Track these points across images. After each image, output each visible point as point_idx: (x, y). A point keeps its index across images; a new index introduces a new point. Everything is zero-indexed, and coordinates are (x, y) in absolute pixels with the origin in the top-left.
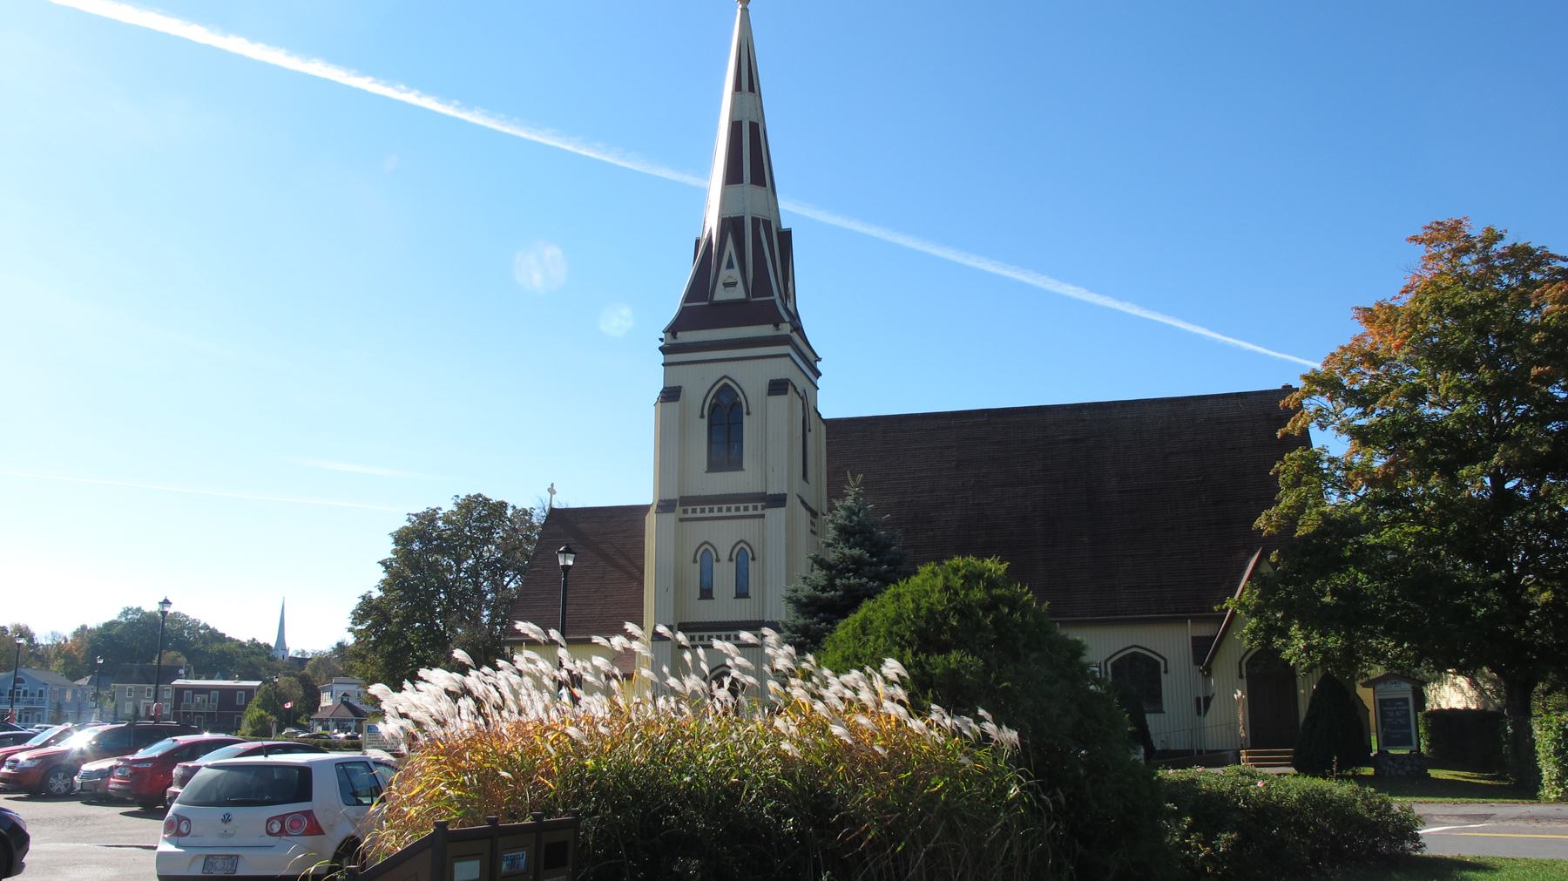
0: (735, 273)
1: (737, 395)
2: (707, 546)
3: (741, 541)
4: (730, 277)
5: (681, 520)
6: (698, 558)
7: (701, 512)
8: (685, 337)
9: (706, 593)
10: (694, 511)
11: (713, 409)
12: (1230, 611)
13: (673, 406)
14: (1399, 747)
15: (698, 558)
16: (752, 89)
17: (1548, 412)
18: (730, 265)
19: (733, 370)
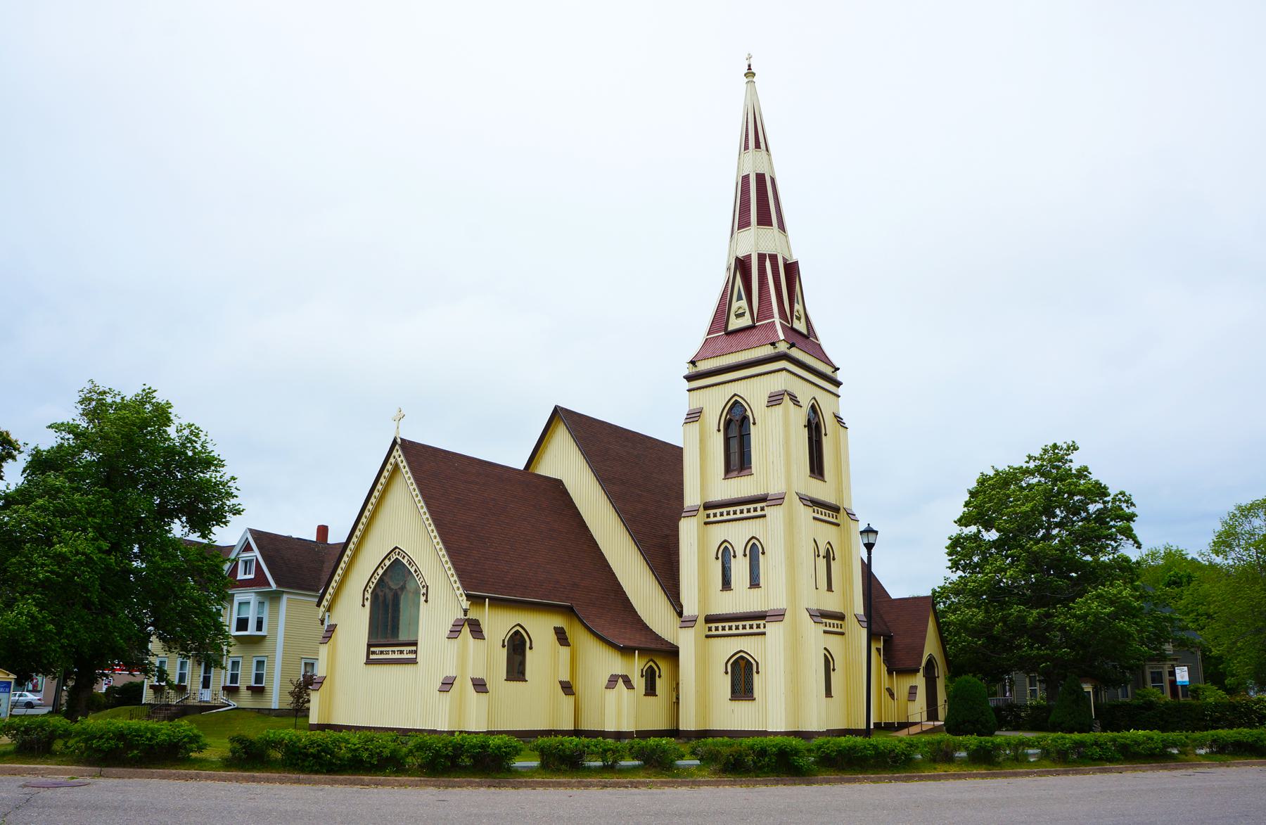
0: (744, 303)
3: (753, 538)
4: (740, 308)
5: (706, 523)
8: (704, 366)
12: (1180, 695)
13: (695, 427)
16: (758, 146)
18: (740, 298)
19: (739, 388)
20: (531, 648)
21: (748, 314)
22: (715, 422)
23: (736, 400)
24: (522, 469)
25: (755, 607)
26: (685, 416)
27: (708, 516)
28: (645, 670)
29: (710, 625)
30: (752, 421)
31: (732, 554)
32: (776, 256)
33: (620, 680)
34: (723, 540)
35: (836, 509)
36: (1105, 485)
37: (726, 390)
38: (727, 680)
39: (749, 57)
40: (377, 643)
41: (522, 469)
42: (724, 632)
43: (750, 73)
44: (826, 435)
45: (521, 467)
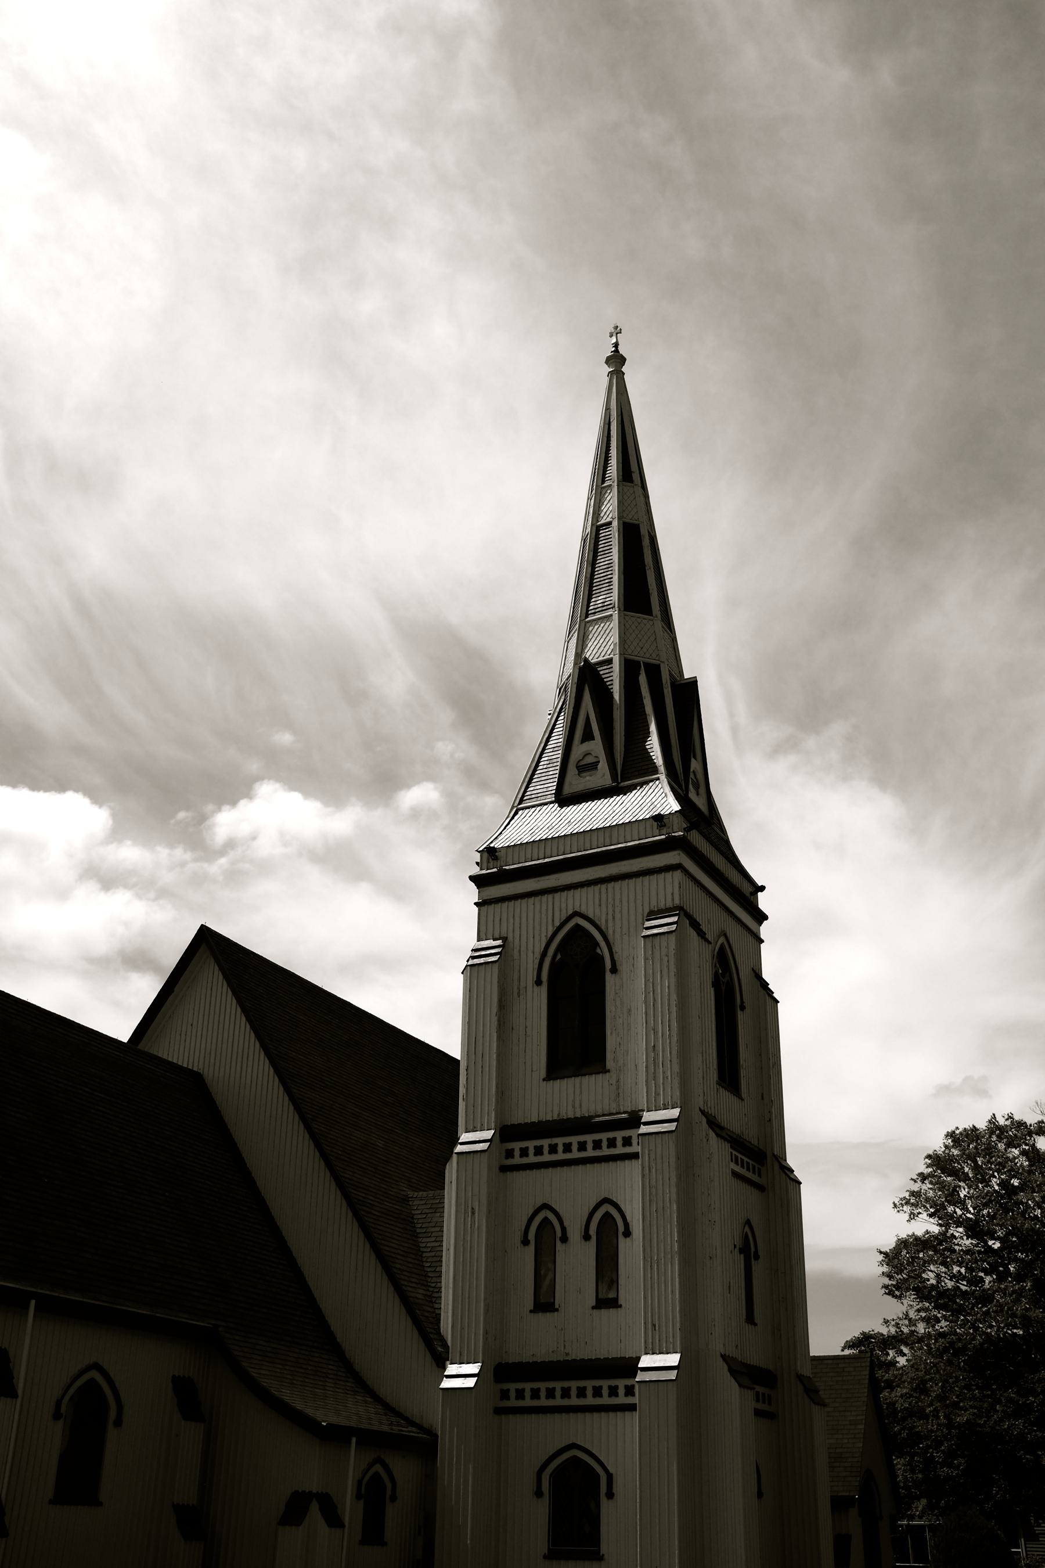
0: (596, 747)
1: (597, 944)
2: (606, 1208)
4: (588, 754)
6: (531, 1236)
7: (624, 1145)
9: (544, 1305)
10: (553, 1149)
11: (556, 969)
14: (622, 577)
15: (531, 1236)
17: (1027, 1148)
20: (118, 1423)
21: (603, 766)
22: (530, 961)
23: (577, 925)
24: (126, 1041)
26: (470, 953)
27: (510, 1154)
29: (505, 1386)
30: (608, 964)
31: (559, 1234)
32: (657, 668)
33: (315, 1507)
34: (539, 1203)
36: (913, 1202)
37: (557, 904)
38: (541, 1511)
39: (617, 331)
40: (599, 1291)
41: (126, 1041)
42: (551, 1403)
43: (617, 360)
44: (743, 1008)
45: (124, 1035)
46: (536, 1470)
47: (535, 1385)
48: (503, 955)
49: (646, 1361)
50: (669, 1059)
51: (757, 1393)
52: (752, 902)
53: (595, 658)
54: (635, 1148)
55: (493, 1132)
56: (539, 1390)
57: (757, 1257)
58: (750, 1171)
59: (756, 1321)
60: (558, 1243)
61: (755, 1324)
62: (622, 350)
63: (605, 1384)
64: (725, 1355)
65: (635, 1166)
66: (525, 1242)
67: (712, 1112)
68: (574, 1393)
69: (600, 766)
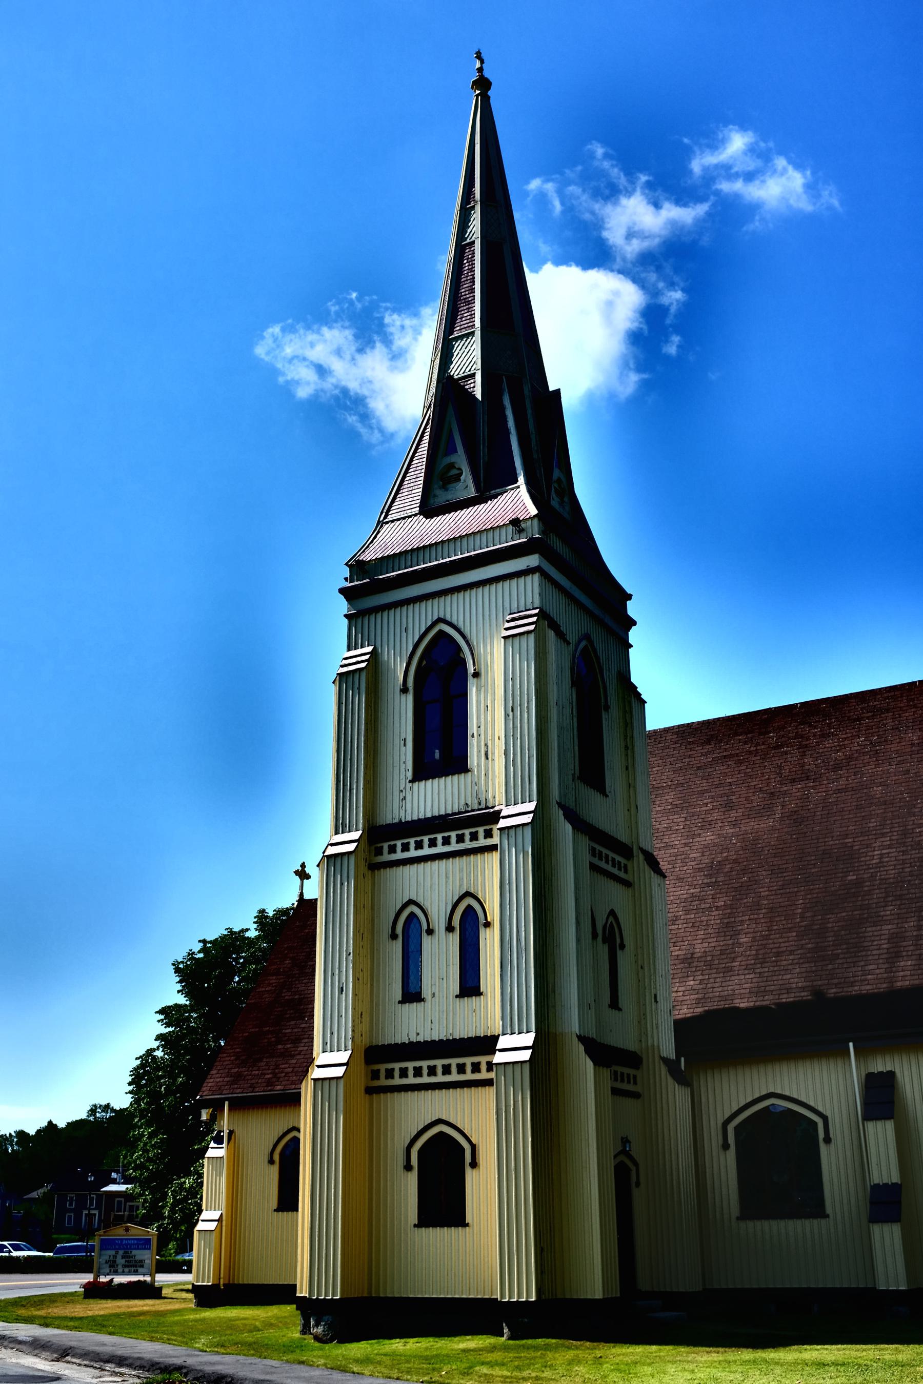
25: (428, 1032)
28: (633, 1168)
29: (376, 1067)
31: (425, 926)
35: (625, 851)
42: (433, 1080)
43: (483, 84)
46: (406, 1145)
47: (418, 1064)
48: (371, 662)
49: (502, 1043)
50: (511, 734)
51: (616, 1073)
52: (781, 1112)
53: (460, 373)
54: (495, 840)
55: (360, 832)
56: (421, 1068)
57: (622, 946)
58: (608, 864)
59: (620, 1006)
60: (424, 934)
61: (620, 1010)
62: (487, 74)
63: (468, 1061)
64: (580, 1035)
65: (496, 856)
66: (394, 936)
67: (572, 805)
68: (454, 1069)
69: (462, 478)
